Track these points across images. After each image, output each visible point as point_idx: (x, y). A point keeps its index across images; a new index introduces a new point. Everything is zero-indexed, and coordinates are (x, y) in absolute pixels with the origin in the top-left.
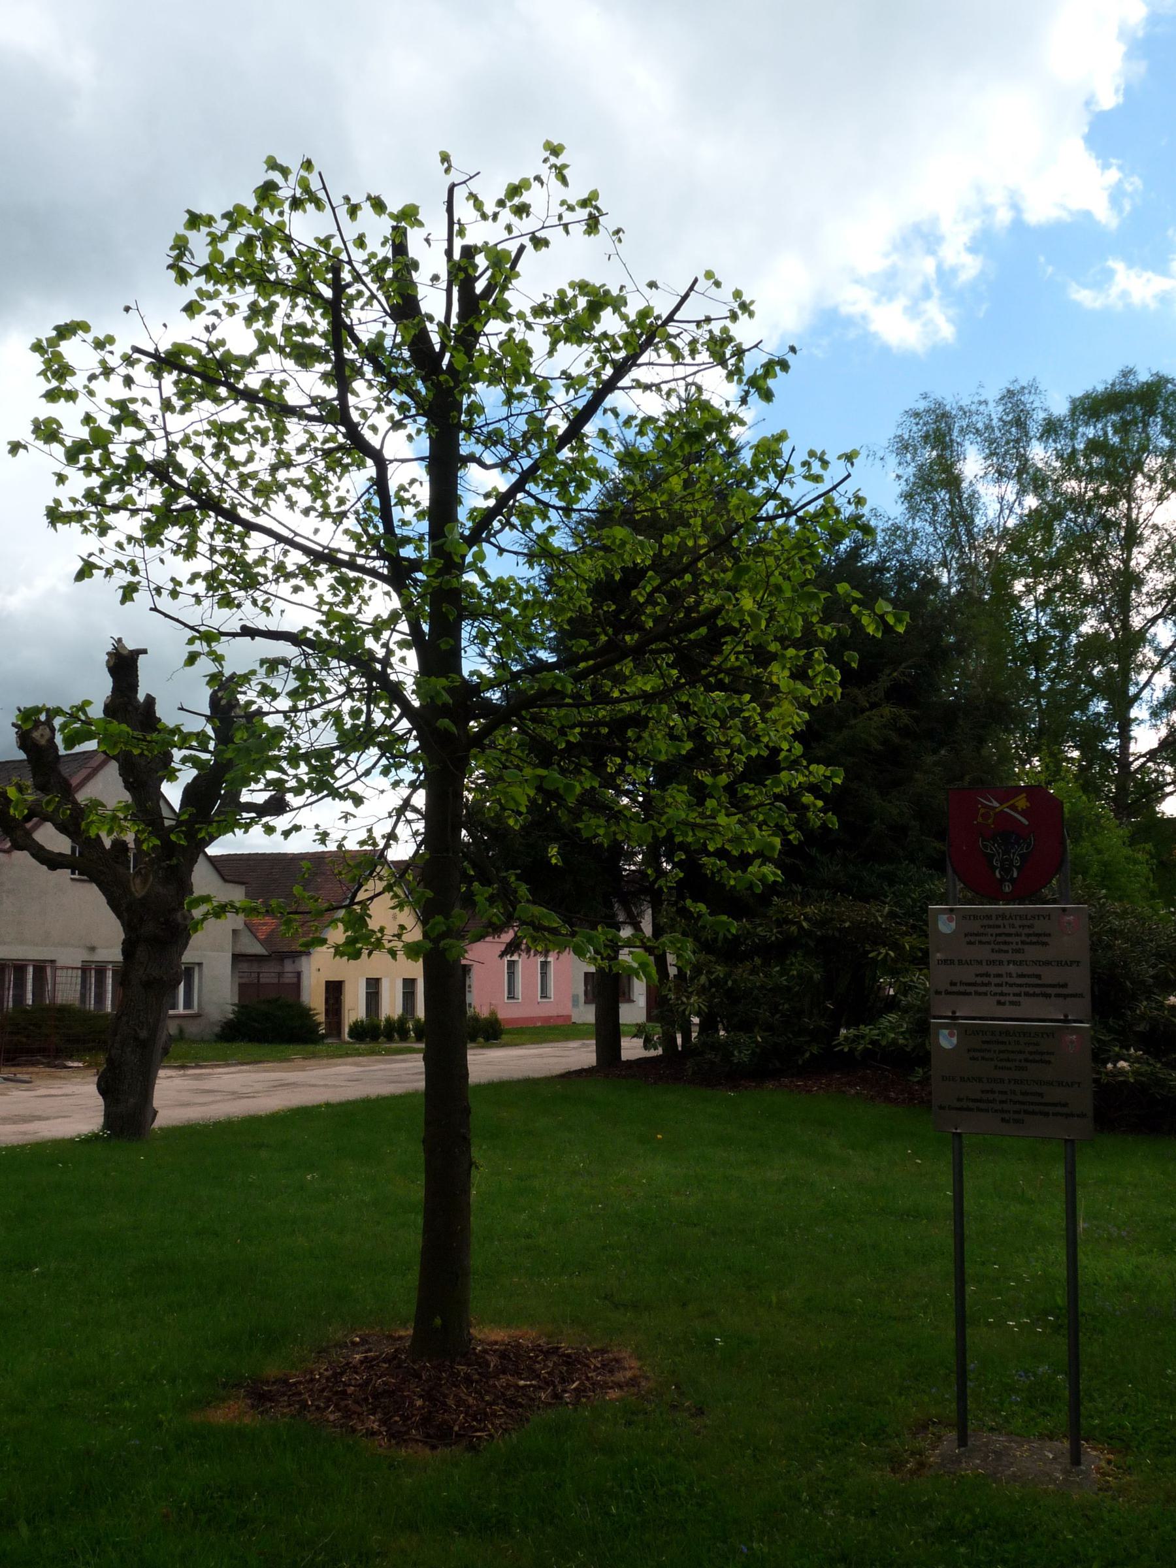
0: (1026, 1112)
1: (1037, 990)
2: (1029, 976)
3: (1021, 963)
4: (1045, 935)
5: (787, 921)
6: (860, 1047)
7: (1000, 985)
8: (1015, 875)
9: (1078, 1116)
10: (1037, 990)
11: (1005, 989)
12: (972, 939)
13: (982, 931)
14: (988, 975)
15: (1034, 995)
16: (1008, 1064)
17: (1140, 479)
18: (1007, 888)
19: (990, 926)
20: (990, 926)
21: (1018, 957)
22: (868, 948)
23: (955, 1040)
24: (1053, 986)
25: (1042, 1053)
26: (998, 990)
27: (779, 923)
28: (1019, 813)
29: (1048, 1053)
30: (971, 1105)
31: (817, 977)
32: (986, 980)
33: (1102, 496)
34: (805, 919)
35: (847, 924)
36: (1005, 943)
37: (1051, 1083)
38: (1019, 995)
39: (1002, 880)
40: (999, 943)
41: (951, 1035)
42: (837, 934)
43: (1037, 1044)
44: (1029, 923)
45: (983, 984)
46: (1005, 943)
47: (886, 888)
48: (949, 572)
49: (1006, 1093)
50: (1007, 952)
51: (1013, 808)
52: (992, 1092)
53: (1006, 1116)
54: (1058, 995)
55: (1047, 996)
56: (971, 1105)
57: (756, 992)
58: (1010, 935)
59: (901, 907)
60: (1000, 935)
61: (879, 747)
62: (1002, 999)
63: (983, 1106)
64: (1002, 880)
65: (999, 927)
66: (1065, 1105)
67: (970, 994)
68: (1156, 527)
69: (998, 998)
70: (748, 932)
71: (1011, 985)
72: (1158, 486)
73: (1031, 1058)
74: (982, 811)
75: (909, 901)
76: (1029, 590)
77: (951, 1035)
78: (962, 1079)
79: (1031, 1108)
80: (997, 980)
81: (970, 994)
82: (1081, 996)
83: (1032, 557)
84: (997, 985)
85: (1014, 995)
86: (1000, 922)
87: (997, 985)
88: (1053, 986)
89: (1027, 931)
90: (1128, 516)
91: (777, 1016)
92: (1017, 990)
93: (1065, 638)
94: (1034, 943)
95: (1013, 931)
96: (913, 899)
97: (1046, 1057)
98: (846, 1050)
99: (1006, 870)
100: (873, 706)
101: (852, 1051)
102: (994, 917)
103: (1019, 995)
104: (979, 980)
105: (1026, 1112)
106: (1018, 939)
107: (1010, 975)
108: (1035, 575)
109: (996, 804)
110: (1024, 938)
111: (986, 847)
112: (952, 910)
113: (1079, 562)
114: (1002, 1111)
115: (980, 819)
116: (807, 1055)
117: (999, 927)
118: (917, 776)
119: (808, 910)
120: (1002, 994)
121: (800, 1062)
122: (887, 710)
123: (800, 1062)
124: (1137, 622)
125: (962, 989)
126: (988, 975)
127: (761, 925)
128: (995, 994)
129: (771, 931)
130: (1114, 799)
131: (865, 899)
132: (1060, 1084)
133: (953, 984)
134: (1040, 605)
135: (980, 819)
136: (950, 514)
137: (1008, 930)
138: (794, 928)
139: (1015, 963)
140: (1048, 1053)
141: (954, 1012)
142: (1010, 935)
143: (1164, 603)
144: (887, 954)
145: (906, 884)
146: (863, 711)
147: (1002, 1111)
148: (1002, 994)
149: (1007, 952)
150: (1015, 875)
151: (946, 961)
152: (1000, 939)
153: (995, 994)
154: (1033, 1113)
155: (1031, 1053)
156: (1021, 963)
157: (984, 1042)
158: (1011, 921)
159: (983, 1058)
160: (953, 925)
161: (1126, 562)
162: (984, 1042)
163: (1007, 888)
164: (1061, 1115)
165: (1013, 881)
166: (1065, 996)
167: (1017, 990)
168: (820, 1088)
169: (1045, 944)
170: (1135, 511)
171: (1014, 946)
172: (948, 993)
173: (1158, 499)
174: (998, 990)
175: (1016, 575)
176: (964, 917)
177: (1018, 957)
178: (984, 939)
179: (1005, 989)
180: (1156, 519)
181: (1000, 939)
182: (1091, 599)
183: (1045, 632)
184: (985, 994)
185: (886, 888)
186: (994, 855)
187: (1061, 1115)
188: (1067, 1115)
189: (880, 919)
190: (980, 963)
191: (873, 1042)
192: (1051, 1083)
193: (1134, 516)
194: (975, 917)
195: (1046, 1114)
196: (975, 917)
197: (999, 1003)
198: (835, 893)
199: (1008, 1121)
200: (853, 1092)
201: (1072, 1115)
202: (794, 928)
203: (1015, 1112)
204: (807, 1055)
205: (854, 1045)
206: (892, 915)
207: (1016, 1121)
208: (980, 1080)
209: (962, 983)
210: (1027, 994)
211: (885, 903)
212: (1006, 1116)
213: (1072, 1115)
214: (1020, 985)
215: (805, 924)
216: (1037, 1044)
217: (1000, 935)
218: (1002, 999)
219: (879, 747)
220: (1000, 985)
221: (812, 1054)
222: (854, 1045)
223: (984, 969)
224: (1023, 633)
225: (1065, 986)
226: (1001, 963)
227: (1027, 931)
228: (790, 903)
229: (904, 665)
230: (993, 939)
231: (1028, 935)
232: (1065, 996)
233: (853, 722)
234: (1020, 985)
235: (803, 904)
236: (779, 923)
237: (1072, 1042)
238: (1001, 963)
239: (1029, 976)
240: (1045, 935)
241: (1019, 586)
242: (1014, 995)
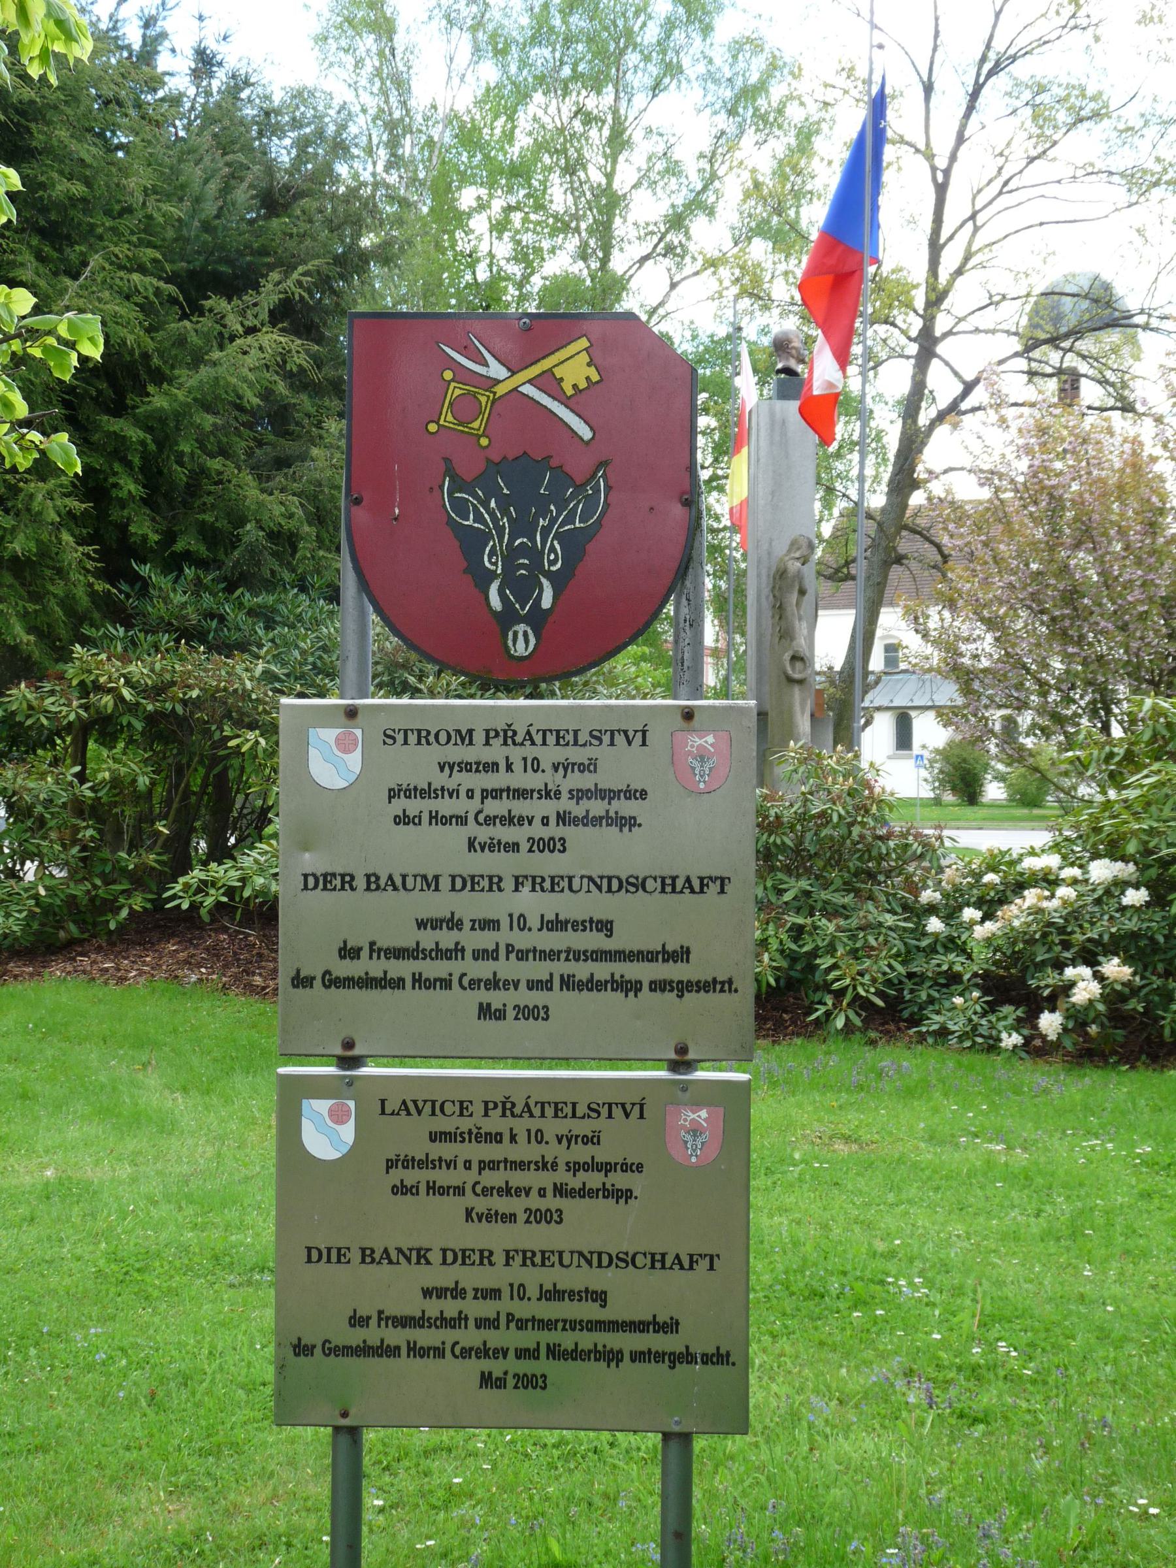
0: (554, 1352)
1: (602, 971)
2: (578, 926)
3: (554, 884)
4: (630, 794)
5: (98, 688)
6: (209, 901)
7: (490, 955)
8: (547, 602)
9: (707, 1359)
10: (602, 971)
11: (507, 968)
12: (414, 806)
13: (441, 780)
14: (454, 923)
15: (592, 985)
16: (502, 1204)
17: (632, 58)
18: (522, 643)
19: (465, 767)
20: (465, 767)
21: (548, 864)
22: (228, 732)
23: (347, 1132)
24: (648, 956)
25: (607, 1168)
26: (484, 969)
27: (84, 690)
28: (566, 402)
29: (626, 1167)
30: (396, 1337)
31: (143, 781)
32: (447, 939)
33: (582, 75)
34: (128, 683)
35: (195, 693)
36: (509, 820)
37: (628, 1260)
38: (546, 985)
39: (508, 618)
40: (490, 820)
41: (338, 1116)
42: (179, 709)
43: (592, 1139)
44: (577, 755)
45: (440, 953)
46: (509, 820)
47: (261, 632)
48: (374, 164)
49: (495, 1293)
50: (515, 847)
51: (549, 383)
52: (457, 1292)
53: (496, 1367)
54: (658, 986)
55: (630, 987)
56: (396, 1337)
57: (39, 809)
58: (521, 794)
59: (284, 664)
60: (496, 794)
61: (256, 401)
62: (496, 999)
63: (426, 1337)
64: (508, 618)
65: (493, 767)
66: (671, 1326)
67: (399, 983)
68: (648, 131)
69: (483, 996)
70: (31, 707)
71: (522, 955)
72: (654, 70)
73: (575, 1183)
74: (455, 391)
75: (296, 653)
76: (482, 206)
77: (338, 1116)
78: (367, 1255)
79: (567, 1340)
80: (485, 940)
81: (399, 983)
82: (727, 986)
83: (487, 157)
84: (481, 955)
85: (532, 985)
86: (496, 752)
87: (481, 955)
88: (648, 956)
89: (576, 780)
90: (615, 111)
91: (75, 850)
92: (539, 970)
93: (526, 279)
94: (597, 821)
95: (533, 781)
96: (303, 653)
97: (619, 1180)
98: (185, 906)
99: (524, 588)
100: (251, 331)
101: (194, 907)
102: (479, 737)
103: (546, 985)
104: (428, 939)
105: (554, 1352)
106: (549, 808)
107: (522, 923)
108: (491, 185)
109: (496, 370)
110: (565, 804)
111: (461, 508)
112: (352, 713)
113: (550, 169)
114: (484, 1352)
115: (447, 419)
116: (124, 913)
117: (493, 767)
118: (315, 452)
119: (132, 668)
120: (494, 983)
121: (112, 926)
122: (271, 339)
123: (112, 926)
124: (619, 263)
125: (376, 968)
126: (454, 923)
127: (52, 693)
128: (475, 984)
129: (70, 705)
130: (166, 744)
131: (226, 648)
132: (657, 1261)
133: (348, 952)
134: (499, 227)
135: (447, 419)
136: (378, 72)
137: (521, 779)
138: (107, 700)
139: (537, 883)
140: (626, 1167)
141: (349, 1045)
142: (521, 794)
143: (655, 239)
144: (257, 742)
145: (292, 626)
146: (232, 338)
147: (484, 1352)
148: (494, 983)
149: (515, 847)
150: (547, 602)
151: (328, 878)
152: (494, 807)
153: (475, 984)
154: (575, 1354)
155: (575, 1167)
156: (554, 884)
157: (434, 1137)
158: (529, 751)
159: (432, 1188)
160: (355, 760)
161: (610, 176)
162: (434, 1137)
163: (522, 643)
164: (659, 1357)
165: (537, 619)
166: (682, 988)
167: (539, 970)
168: (141, 973)
169: (630, 823)
170: (623, 104)
171: (538, 830)
172: (332, 982)
173: (654, 89)
174: (484, 969)
175: (466, 179)
176: (389, 737)
177: (548, 864)
178: (446, 807)
179: (507, 968)
180: (647, 120)
181: (494, 807)
182: (563, 225)
183: (500, 269)
184: (446, 984)
185: (261, 632)
186: (485, 537)
187: (659, 1357)
188: (675, 1359)
189: (249, 685)
190: (431, 883)
191: (230, 892)
192: (628, 1260)
193: (622, 112)
194: (424, 737)
195: (613, 1357)
196: (424, 737)
197: (485, 1011)
198: (177, 641)
199: (500, 1383)
200: (194, 978)
201: (687, 1357)
202: (107, 700)
203: (522, 1354)
204: (124, 913)
205: (198, 898)
206: (268, 676)
207: (528, 1382)
208: (422, 1256)
209: (374, 949)
210: (568, 983)
211: (258, 657)
212: (496, 1367)
213: (687, 1357)
214: (551, 955)
215: (126, 693)
216: (592, 1139)
217: (496, 794)
218: (496, 999)
219: (256, 401)
220: (490, 955)
221: (132, 912)
222: (198, 898)
223: (440, 904)
224: (472, 266)
225: (682, 955)
226: (495, 883)
227: (576, 780)
228: (103, 656)
229: (300, 269)
230: (475, 804)
231: (579, 795)
232: (682, 988)
233: (216, 355)
234: (551, 955)
235: (125, 659)
236: (84, 690)
237: (695, 1131)
238: (495, 883)
239: (578, 926)
240: (630, 794)
241: (467, 197)
242: (532, 985)
